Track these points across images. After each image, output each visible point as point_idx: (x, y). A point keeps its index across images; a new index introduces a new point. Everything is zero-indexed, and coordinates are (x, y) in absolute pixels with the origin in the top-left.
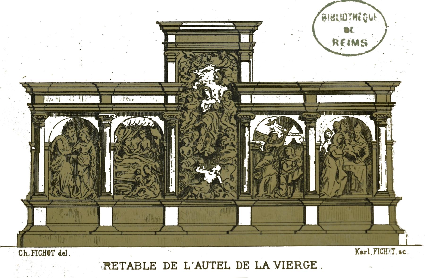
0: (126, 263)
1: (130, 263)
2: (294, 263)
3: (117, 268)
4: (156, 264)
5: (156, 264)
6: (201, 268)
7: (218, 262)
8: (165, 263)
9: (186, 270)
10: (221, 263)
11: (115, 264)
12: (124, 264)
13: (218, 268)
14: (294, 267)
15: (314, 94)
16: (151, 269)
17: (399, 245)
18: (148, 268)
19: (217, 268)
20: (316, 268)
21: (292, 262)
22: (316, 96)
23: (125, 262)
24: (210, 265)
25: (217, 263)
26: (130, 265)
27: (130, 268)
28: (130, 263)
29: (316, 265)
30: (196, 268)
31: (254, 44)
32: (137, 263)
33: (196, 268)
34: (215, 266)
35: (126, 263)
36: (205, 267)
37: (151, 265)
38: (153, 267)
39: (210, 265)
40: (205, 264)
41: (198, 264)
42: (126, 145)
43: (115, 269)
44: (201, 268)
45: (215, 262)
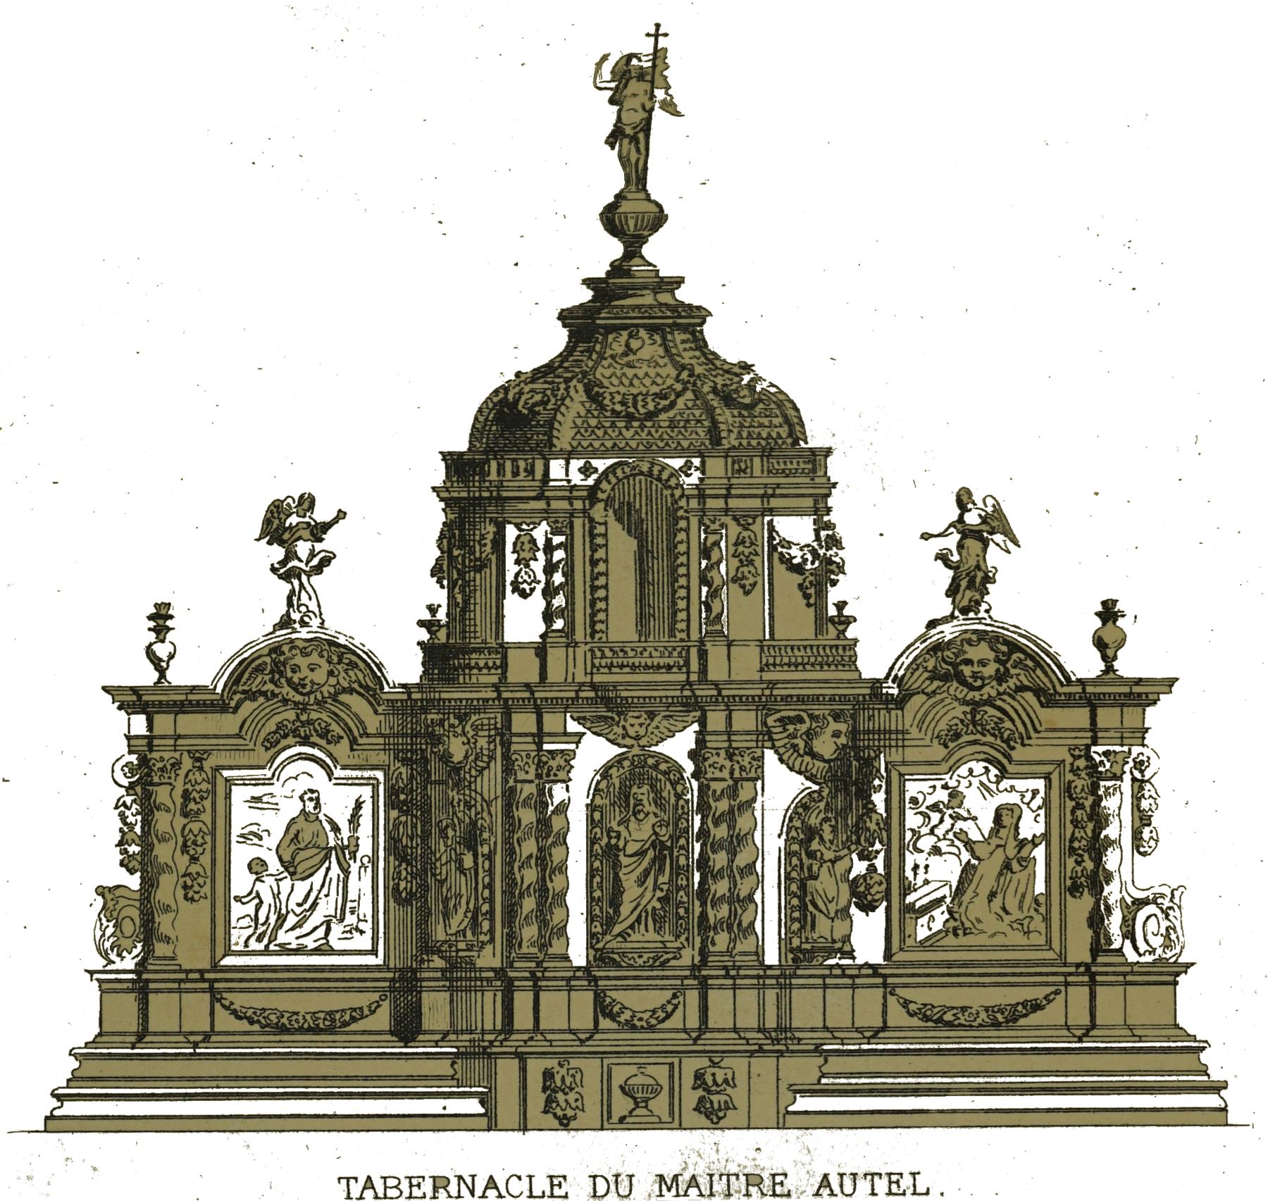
0: (356, 1179)
1: (369, 1178)
2: (429, 1183)
3: (421, 1195)
4: (565, 1180)
5: (565, 1180)
6: (832, 1194)
7: (889, 1174)
8: (595, 1177)
9: (532, 1200)
10: (782, 1178)
11: (415, 1182)
12: (352, 1182)
13: (890, 1193)
14: (430, 1193)
15: (1136, 705)
16: (552, 1196)
17: (1227, 1125)
18: (543, 1192)
19: (887, 1191)
20: (566, 1196)
21: (901, 1174)
22: (1144, 710)
23: (876, 1174)
24: (864, 1186)
25: (885, 1180)
26: (693, 1183)
27: (825, 1192)
28: (369, 1178)
29: (790, 1184)
30: (817, 1194)
31: (980, 575)
32: (388, 1180)
33: (817, 1194)
34: (882, 1185)
35: (356, 1179)
36: (849, 1189)
37: (552, 1185)
38: (557, 1191)
39: (864, 1186)
40: (848, 1182)
41: (825, 1181)
42: (1003, 857)
43: (781, 1196)
44: (832, 1194)
45: (880, 1175)
